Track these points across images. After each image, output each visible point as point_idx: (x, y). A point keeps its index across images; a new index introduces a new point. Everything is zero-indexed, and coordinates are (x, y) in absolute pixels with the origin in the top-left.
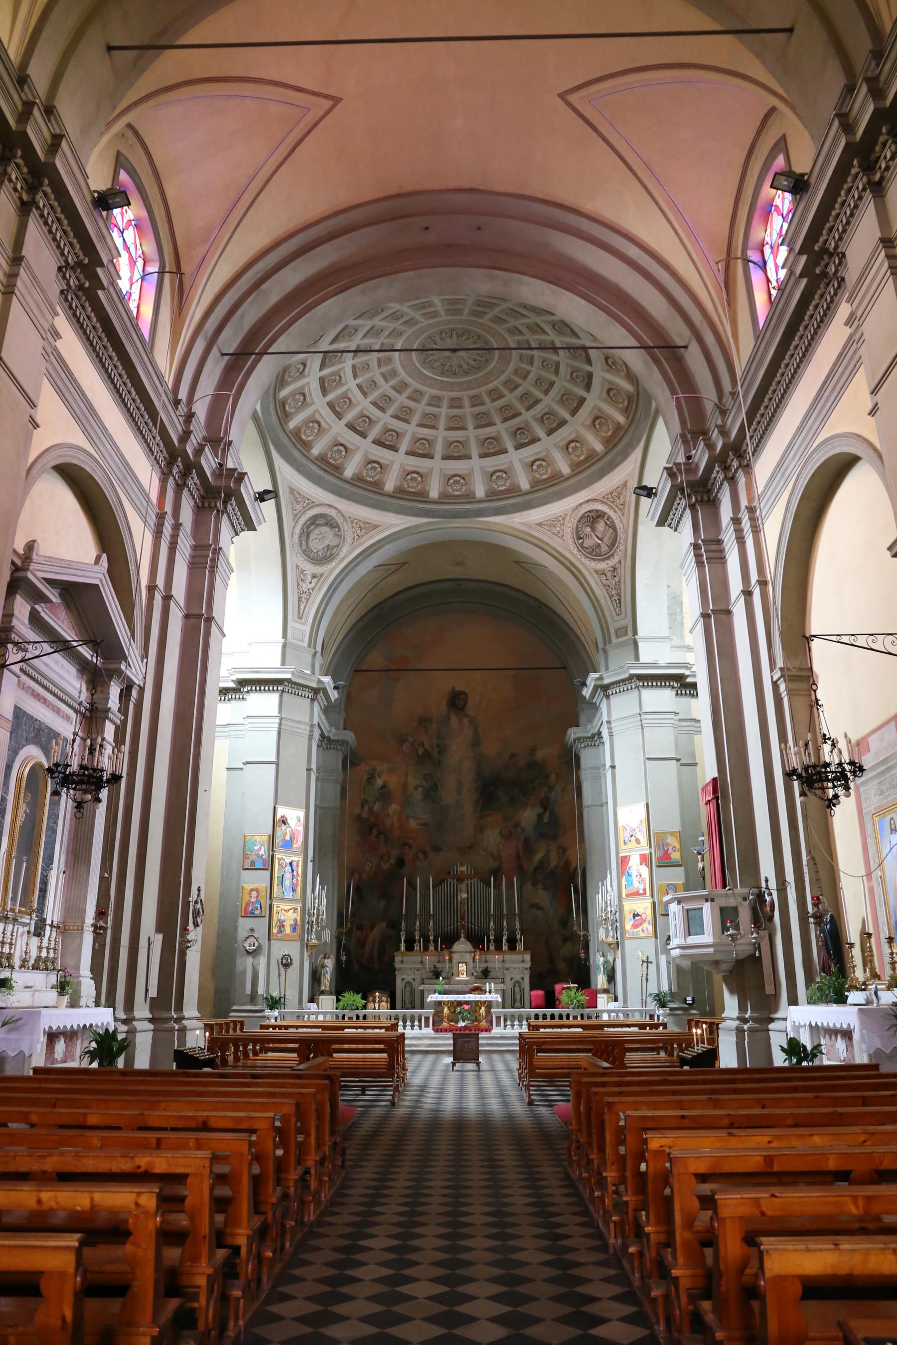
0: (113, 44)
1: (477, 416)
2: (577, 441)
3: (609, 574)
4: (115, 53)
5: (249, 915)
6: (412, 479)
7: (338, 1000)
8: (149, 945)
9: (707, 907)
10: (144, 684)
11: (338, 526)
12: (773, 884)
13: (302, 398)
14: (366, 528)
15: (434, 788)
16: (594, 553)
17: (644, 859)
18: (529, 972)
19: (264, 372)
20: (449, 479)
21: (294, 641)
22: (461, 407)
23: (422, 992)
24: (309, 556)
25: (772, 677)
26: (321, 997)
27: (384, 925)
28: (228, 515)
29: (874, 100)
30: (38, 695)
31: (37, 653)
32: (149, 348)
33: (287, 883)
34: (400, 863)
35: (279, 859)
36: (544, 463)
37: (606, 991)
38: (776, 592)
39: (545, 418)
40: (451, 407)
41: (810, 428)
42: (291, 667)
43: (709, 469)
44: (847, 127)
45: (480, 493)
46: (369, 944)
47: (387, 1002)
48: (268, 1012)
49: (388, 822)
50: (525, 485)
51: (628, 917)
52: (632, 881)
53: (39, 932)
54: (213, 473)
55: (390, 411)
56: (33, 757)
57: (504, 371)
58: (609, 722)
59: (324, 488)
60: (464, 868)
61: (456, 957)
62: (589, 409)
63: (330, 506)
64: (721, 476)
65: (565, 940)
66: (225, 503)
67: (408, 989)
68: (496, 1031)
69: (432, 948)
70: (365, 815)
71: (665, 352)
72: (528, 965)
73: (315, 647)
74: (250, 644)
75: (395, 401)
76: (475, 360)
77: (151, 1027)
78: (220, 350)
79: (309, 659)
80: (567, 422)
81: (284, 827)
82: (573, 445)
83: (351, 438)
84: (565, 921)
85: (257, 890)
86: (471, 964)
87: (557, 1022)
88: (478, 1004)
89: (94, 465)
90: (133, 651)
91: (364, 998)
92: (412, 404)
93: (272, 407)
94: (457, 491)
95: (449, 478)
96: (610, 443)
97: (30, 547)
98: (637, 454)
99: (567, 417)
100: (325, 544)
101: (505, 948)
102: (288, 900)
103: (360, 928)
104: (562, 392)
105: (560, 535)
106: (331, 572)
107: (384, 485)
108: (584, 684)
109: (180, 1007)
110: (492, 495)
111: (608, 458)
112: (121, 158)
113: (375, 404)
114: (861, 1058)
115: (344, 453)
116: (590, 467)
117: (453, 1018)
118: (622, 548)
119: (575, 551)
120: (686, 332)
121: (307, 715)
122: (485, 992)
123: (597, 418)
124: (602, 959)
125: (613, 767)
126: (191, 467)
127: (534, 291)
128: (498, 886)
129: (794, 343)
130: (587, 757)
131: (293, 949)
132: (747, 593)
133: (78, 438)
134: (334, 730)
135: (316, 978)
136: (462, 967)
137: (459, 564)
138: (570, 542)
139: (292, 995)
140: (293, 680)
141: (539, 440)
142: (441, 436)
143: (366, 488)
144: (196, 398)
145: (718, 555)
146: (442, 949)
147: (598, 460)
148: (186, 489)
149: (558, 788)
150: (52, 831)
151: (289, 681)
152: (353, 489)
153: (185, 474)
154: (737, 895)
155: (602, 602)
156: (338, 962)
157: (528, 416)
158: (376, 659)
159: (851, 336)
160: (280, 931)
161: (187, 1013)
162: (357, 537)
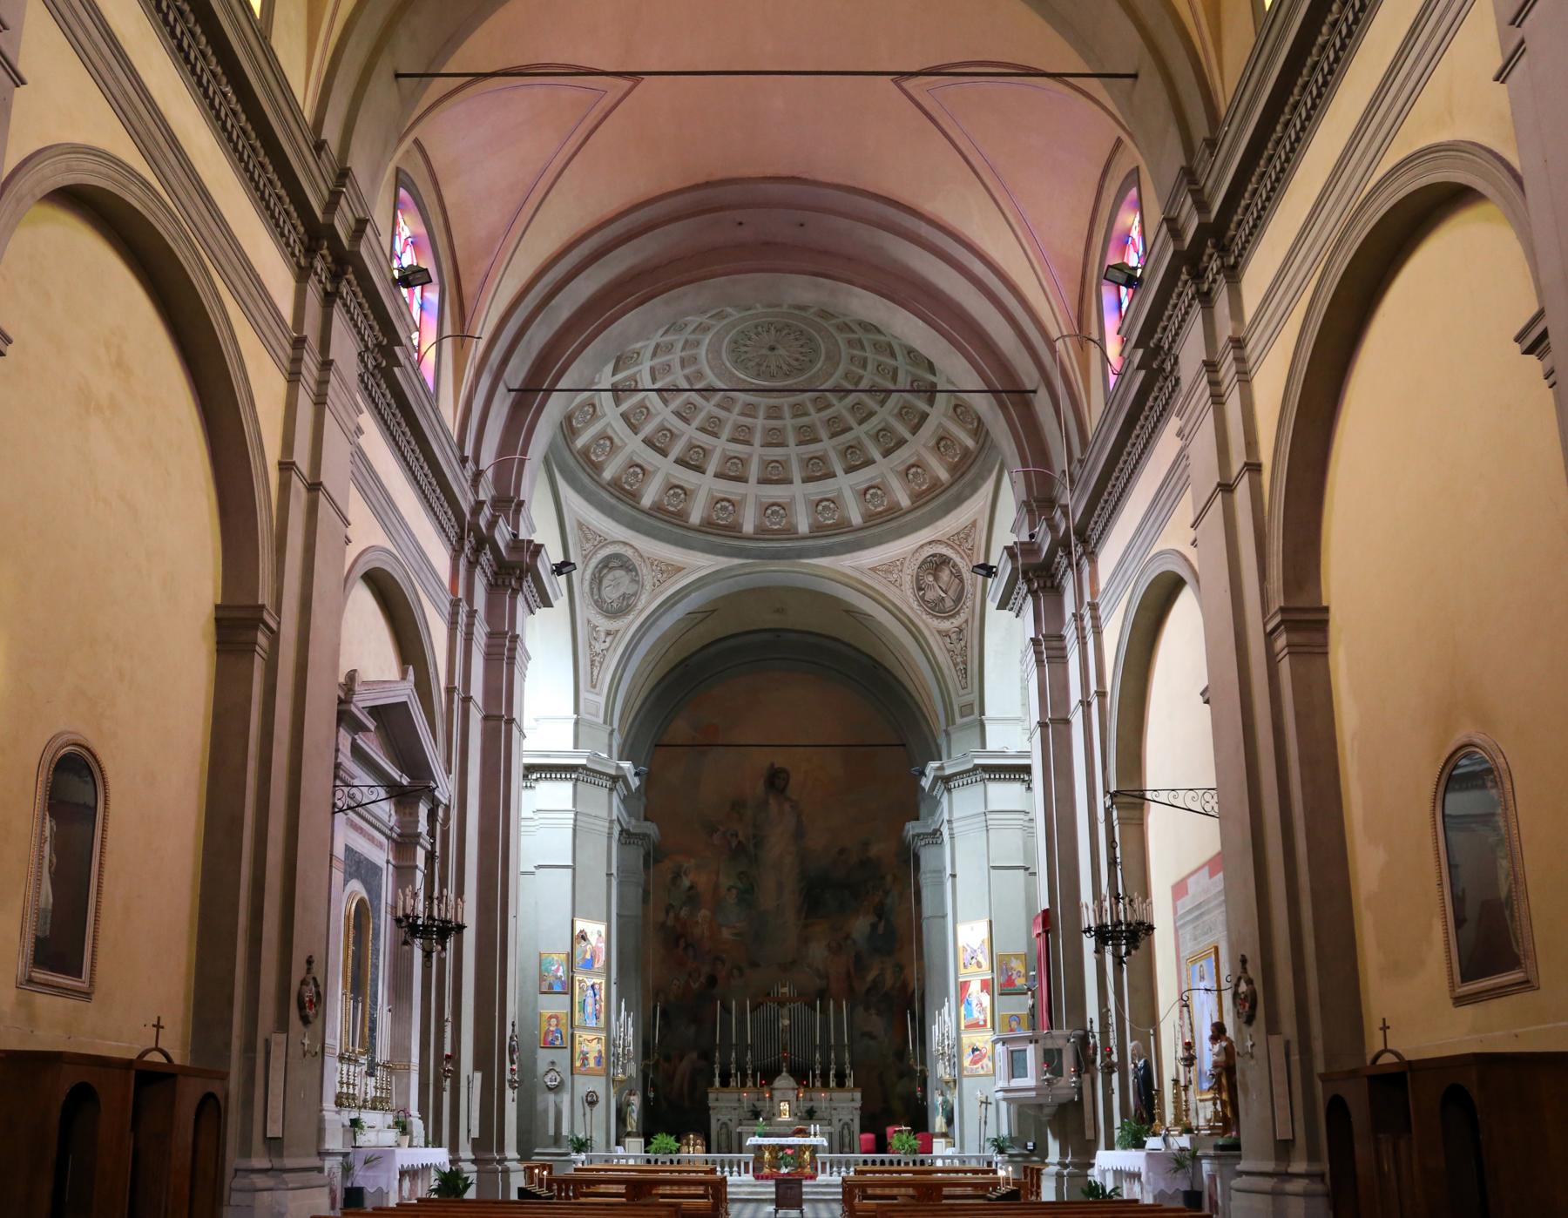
1: (799, 429)
3: (954, 636)
4: (402, 80)
5: (550, 1046)
6: (724, 509)
7: (647, 1143)
9: (1031, 1050)
12: (1096, 1028)
16: (937, 609)
17: (985, 985)
19: (555, 408)
21: (588, 717)
23: (740, 1134)
25: (1265, 625)
26: (628, 1140)
27: (694, 1055)
31: (373, 798)
32: (434, 398)
33: (589, 1009)
34: (712, 981)
37: (944, 1135)
38: (1113, 702)
41: (1408, 75)
42: (587, 752)
44: (1175, 232)
45: (803, 527)
48: (574, 1156)
50: (856, 519)
51: (967, 1051)
53: (371, 1074)
54: (507, 546)
55: (695, 424)
57: (831, 375)
58: (949, 821)
60: (786, 990)
61: (777, 1094)
62: (933, 428)
63: (625, 544)
64: (1065, 562)
65: (901, 1076)
66: (520, 579)
68: (822, 1178)
69: (750, 1084)
70: (670, 923)
71: (1013, 396)
72: (858, 1104)
77: (474, 1168)
81: (583, 944)
83: (649, 457)
84: (901, 1053)
85: (556, 1017)
86: (794, 1104)
87: (887, 1167)
88: (801, 1149)
91: (678, 1140)
92: (722, 414)
95: (766, 508)
96: (958, 471)
97: (352, 676)
98: (987, 488)
99: (907, 435)
101: (832, 1084)
103: (667, 1058)
108: (923, 773)
109: (501, 1149)
110: (818, 530)
111: (955, 489)
112: (401, 176)
113: (677, 414)
114: (1148, 1199)
116: (935, 499)
117: (775, 1163)
119: (915, 605)
121: (605, 807)
122: (808, 1135)
123: (942, 438)
124: (940, 1099)
125: (954, 876)
126: (484, 541)
127: (864, 305)
128: (824, 1011)
129: (1136, 432)
130: (927, 856)
131: (598, 1085)
132: (1085, 704)
133: (380, 539)
134: (633, 821)
136: (785, 1106)
137: (779, 611)
138: (909, 593)
139: (598, 1138)
140: (590, 766)
142: (756, 454)
143: (667, 520)
145: (1059, 653)
151: (584, 767)
153: (477, 550)
154: (1063, 1037)
155: (946, 672)
157: (860, 432)
158: (681, 729)
159: (1182, 449)
160: (583, 1065)
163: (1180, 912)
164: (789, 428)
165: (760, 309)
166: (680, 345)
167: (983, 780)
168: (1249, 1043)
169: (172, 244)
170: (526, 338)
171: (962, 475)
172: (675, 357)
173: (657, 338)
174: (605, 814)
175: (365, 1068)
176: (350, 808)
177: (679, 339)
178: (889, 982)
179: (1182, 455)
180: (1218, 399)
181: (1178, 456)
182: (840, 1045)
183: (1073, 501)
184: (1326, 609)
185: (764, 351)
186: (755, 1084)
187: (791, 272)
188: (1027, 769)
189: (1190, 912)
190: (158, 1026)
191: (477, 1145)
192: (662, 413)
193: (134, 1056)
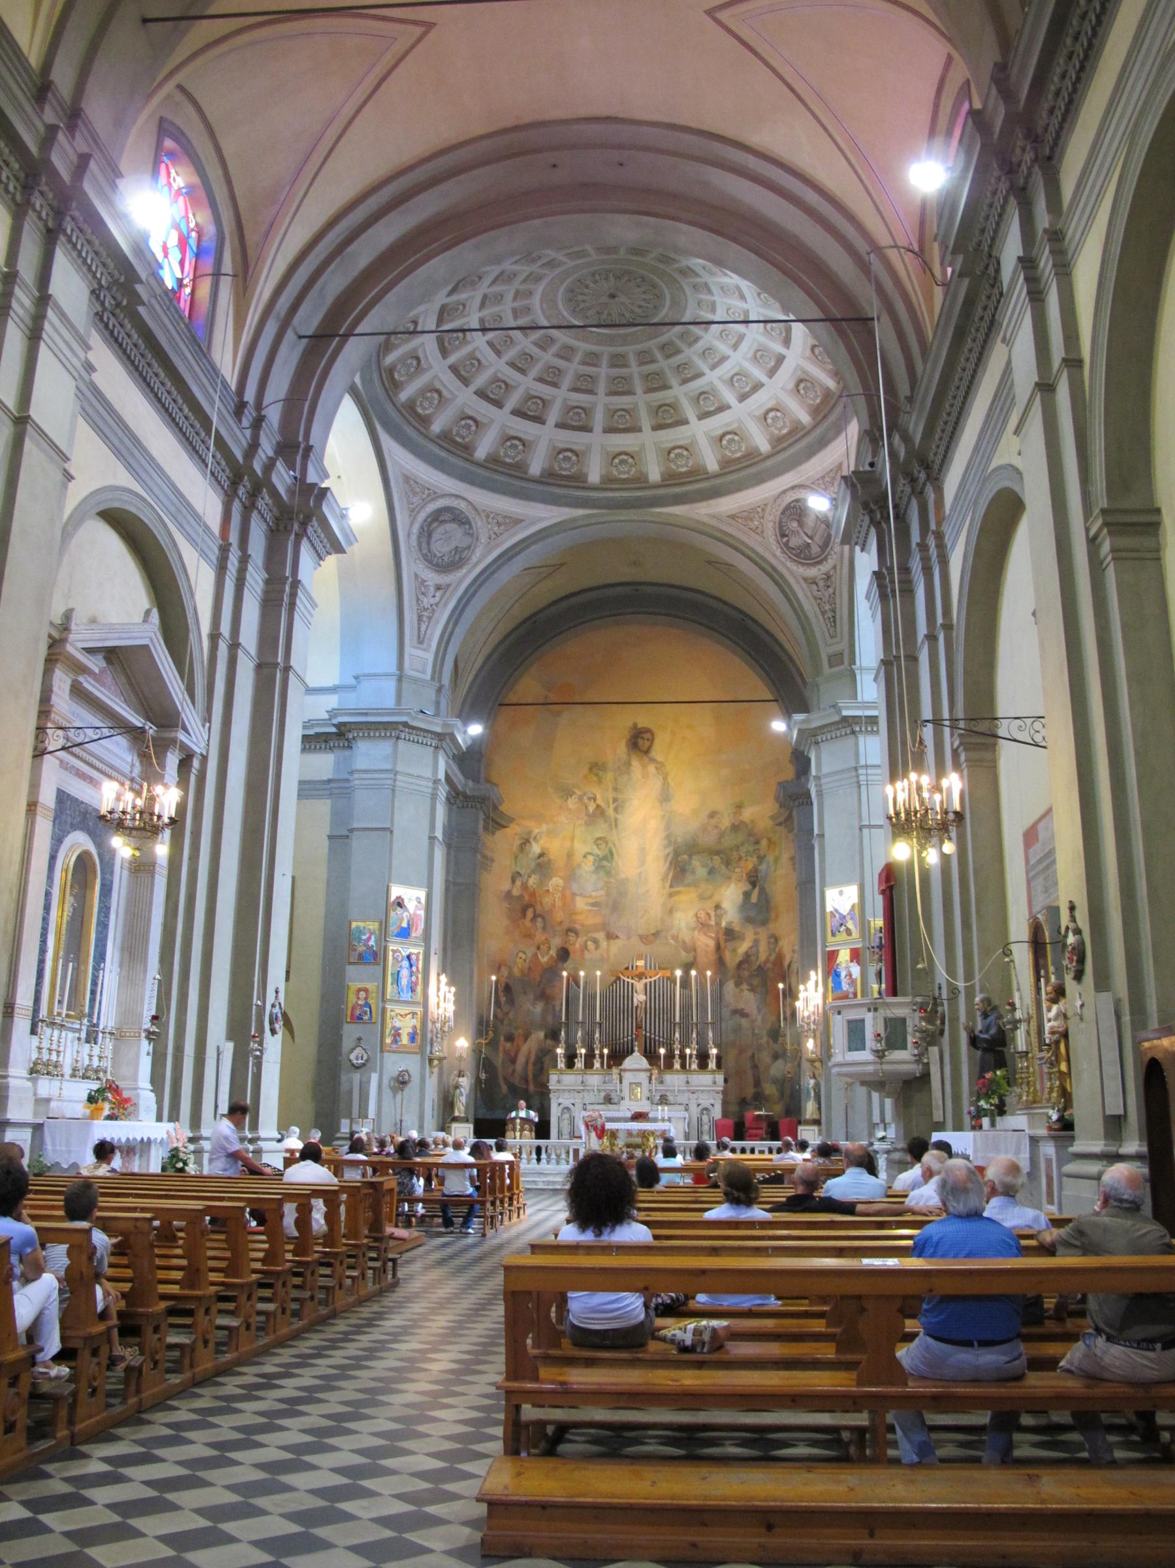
0: (151, 15)
1: (647, 377)
2: (778, 410)
3: (821, 583)
8: (218, 1055)
9: (869, 1017)
10: (208, 751)
11: (468, 522)
13: (415, 363)
14: (506, 524)
15: (610, 856)
18: (721, 1096)
20: (614, 458)
24: (430, 562)
25: (1087, 530)
26: (454, 1125)
27: (541, 1034)
28: (309, 538)
29: (1005, 103)
30: (84, 774)
33: (404, 981)
34: (564, 954)
35: (394, 952)
36: (736, 438)
37: (817, 1122)
39: (735, 379)
40: (613, 365)
46: (521, 1060)
47: (531, 1131)
49: (547, 901)
52: (840, 983)
56: (80, 844)
59: (449, 474)
61: (628, 1077)
64: (908, 490)
65: (776, 1057)
66: (304, 525)
67: (566, 1116)
70: (516, 892)
72: (720, 1086)
73: (440, 680)
74: (356, 678)
75: (538, 360)
76: (640, 307)
78: (296, 333)
79: (431, 694)
80: (763, 385)
82: (772, 414)
83: (483, 409)
85: (366, 990)
89: (140, 504)
90: (190, 715)
92: (561, 363)
93: (375, 376)
94: (624, 473)
97: (68, 615)
99: (763, 378)
100: (453, 546)
102: (405, 1002)
103: (510, 1038)
104: (755, 347)
105: (759, 531)
107: (528, 466)
113: (512, 365)
115: (473, 428)
119: (778, 553)
120: (876, 301)
124: (812, 1082)
133: (123, 478)
134: (470, 783)
138: (772, 540)
141: (729, 407)
143: (503, 472)
144: (265, 404)
146: (609, 1067)
147: (803, 436)
148: (255, 512)
149: (770, 858)
150: (103, 926)
152: (487, 474)
153: (254, 494)
156: (478, 1081)
160: (395, 1041)
161: (263, 1133)
162: (493, 536)
163: (1032, 862)
164: (636, 376)
165: (594, 256)
166: (511, 295)
167: (853, 732)
168: (1079, 1003)
171: (825, 417)
174: (428, 774)
178: (763, 956)
180: (1036, 296)
184: (1158, 511)
185: (605, 299)
189: (1040, 861)
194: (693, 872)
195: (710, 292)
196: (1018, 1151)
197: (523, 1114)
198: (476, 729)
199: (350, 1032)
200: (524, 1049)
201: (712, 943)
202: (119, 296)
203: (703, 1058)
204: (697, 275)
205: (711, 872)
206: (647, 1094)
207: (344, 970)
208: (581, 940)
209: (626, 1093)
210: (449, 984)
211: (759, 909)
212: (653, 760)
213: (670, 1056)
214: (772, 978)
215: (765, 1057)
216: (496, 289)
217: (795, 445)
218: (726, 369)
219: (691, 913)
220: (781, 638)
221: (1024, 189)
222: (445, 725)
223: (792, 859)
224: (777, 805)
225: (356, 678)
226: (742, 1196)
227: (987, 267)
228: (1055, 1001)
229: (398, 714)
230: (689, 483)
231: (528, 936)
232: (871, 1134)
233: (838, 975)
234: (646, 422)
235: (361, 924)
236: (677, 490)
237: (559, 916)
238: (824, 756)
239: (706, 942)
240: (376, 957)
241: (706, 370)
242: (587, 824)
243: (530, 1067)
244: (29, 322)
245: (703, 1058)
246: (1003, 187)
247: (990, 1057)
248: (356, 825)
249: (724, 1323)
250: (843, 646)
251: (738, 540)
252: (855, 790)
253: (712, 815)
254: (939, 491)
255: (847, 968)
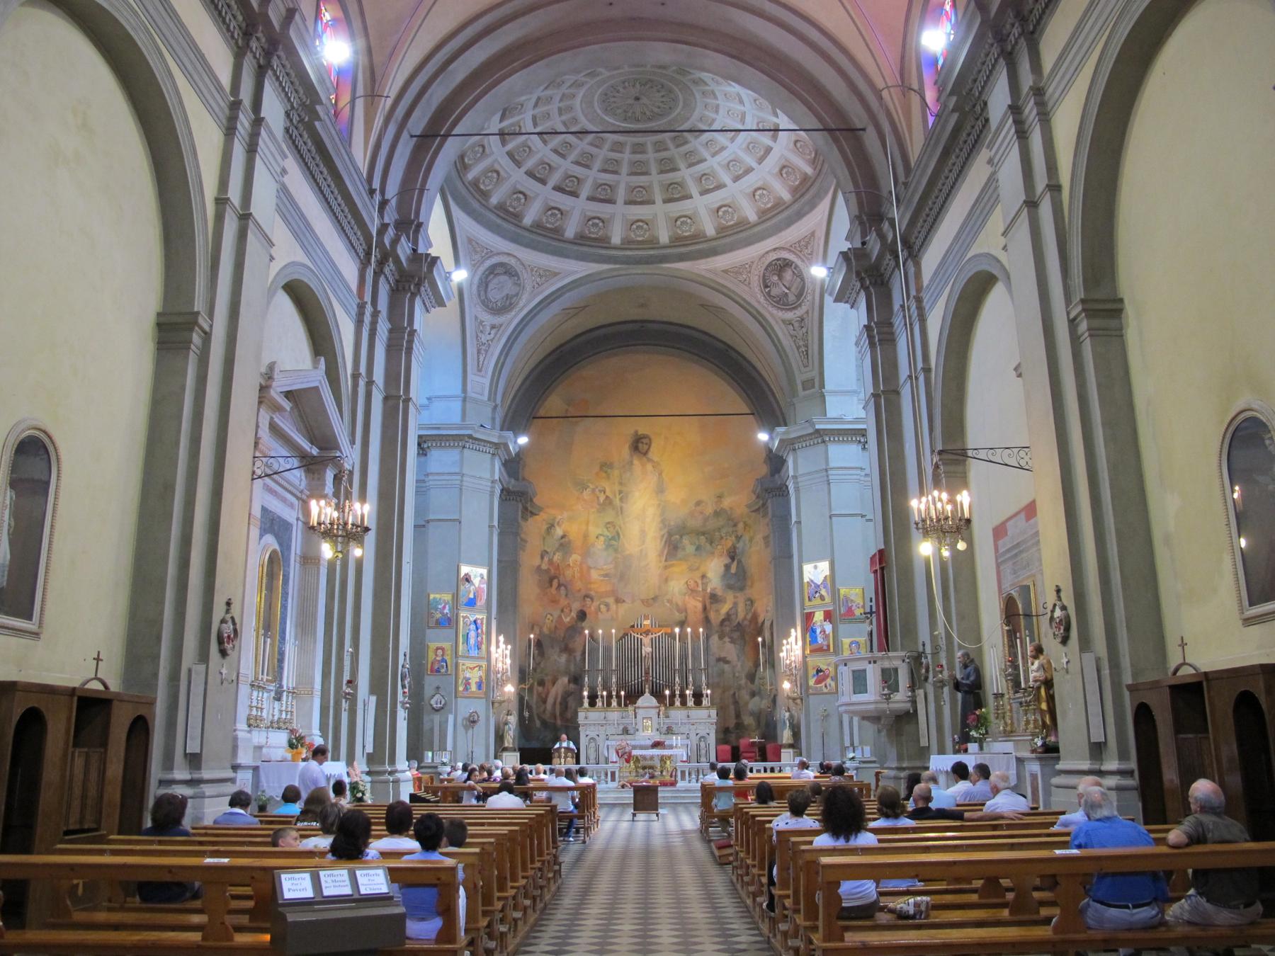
3: (796, 325)
6: (594, 225)
10: (211, 326)
11: (517, 275)
15: (617, 536)
16: (781, 302)
19: (451, 149)
22: (643, 152)
25: (1068, 313)
26: (505, 754)
27: (566, 680)
31: (288, 467)
32: (346, 138)
33: (472, 641)
34: (582, 615)
37: (791, 746)
43: (881, 256)
46: (550, 700)
49: (568, 573)
53: (278, 698)
54: (408, 259)
55: (572, 157)
58: (795, 477)
61: (641, 713)
63: (509, 254)
65: (753, 695)
66: (418, 285)
67: (593, 744)
70: (544, 567)
74: (429, 399)
77: (368, 779)
79: (489, 410)
82: (759, 192)
83: (531, 186)
85: (443, 649)
90: (343, 440)
92: (594, 150)
97: (271, 367)
98: (824, 205)
99: (754, 164)
100: (504, 294)
103: (541, 683)
106: (509, 324)
109: (392, 761)
111: (796, 206)
113: (555, 151)
118: (809, 298)
119: (762, 300)
124: (787, 714)
126: (387, 256)
133: (300, 257)
135: (500, 738)
137: (642, 306)
138: (757, 290)
141: (725, 186)
143: (546, 235)
149: (746, 537)
154: (897, 660)
156: (521, 718)
160: (466, 689)
163: (1001, 550)
165: (627, 69)
167: (824, 442)
168: (1065, 660)
169: (132, 33)
170: (427, 95)
171: (802, 195)
172: (553, 108)
173: (539, 92)
174: (487, 475)
175: (273, 694)
176: (267, 475)
177: (557, 93)
178: (741, 615)
179: (992, 180)
180: (1022, 135)
181: (989, 180)
182: (696, 670)
183: (898, 215)
184: (1121, 300)
185: (631, 101)
186: (619, 704)
187: (655, 40)
188: (863, 433)
189: (1008, 551)
190: (98, 659)
191: (371, 759)
192: (542, 151)
193: (76, 684)
194: (684, 549)
195: (716, 98)
196: (1008, 769)
197: (565, 744)
198: (523, 440)
199: (430, 682)
200: (553, 691)
201: (700, 606)
202: (303, 114)
203: (698, 697)
204: (706, 84)
205: (698, 548)
206: (656, 726)
207: (424, 635)
208: (596, 603)
209: (639, 726)
210: (506, 643)
211: (737, 577)
212: (649, 460)
213: (673, 695)
214: (754, 637)
215: (744, 695)
216: (549, 92)
217: (777, 216)
218: (724, 156)
219: (683, 582)
220: (758, 365)
221: (1011, 53)
222: (500, 437)
223: (766, 538)
224: (754, 497)
225: (429, 399)
226: (889, 812)
227: (974, 106)
228: (1036, 657)
229: (467, 428)
230: (691, 245)
231: (554, 601)
232: (843, 754)
233: (814, 631)
234: (658, 197)
235: (438, 596)
236: (683, 250)
237: (579, 585)
238: (800, 461)
239: (695, 605)
240: (450, 622)
241: (708, 157)
242: (599, 511)
243: (558, 707)
244: (247, 139)
245: (698, 697)
246: (995, 51)
247: (971, 698)
248: (431, 517)
249: (925, 898)
250: (815, 373)
251: (729, 289)
252: (826, 487)
253: (698, 503)
254: (918, 265)
255: (822, 626)
